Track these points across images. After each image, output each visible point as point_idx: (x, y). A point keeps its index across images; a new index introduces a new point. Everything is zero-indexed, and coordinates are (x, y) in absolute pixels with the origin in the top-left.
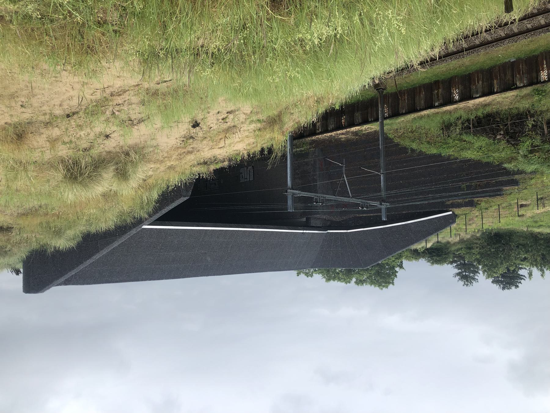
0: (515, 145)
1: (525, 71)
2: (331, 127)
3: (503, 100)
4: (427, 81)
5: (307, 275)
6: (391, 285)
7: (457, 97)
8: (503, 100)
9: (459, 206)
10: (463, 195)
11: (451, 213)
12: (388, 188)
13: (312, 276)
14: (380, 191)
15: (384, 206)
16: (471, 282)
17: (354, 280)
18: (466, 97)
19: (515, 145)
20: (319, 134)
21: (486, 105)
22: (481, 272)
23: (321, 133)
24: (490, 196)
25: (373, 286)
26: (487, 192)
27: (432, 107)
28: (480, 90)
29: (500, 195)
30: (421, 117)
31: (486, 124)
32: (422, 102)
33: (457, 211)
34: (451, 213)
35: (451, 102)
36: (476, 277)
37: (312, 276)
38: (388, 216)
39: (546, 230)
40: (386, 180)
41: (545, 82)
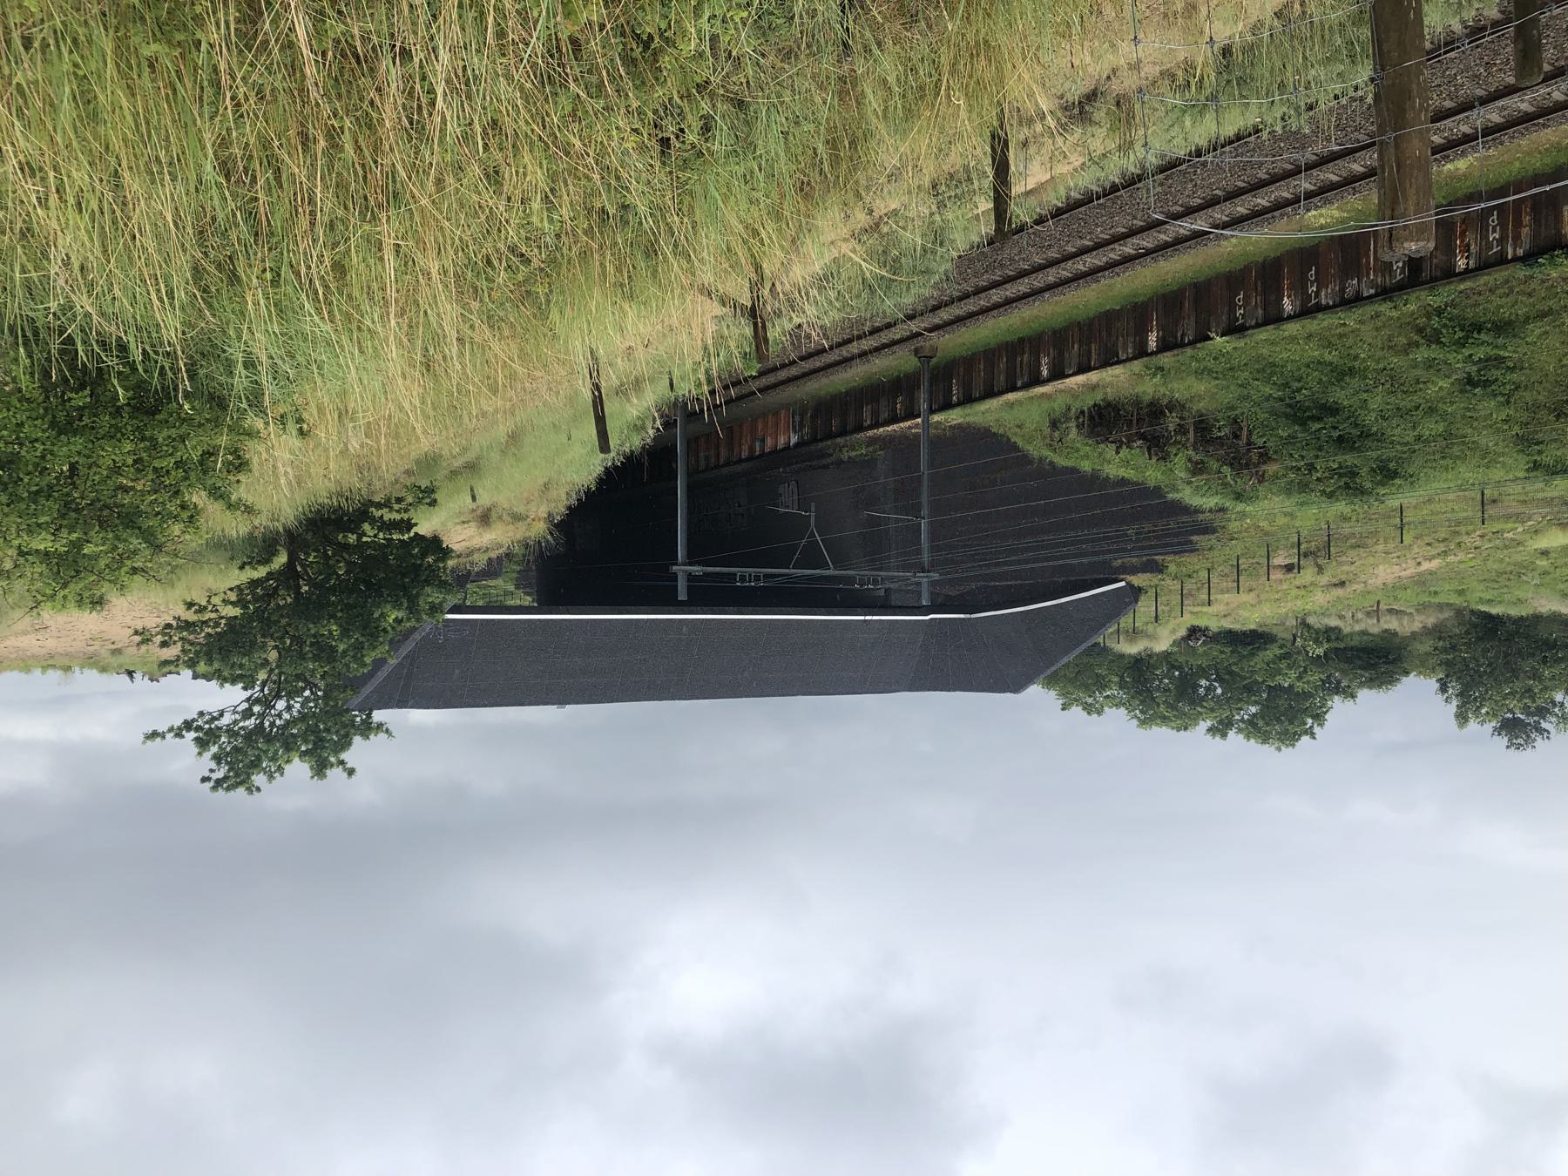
1: (1557, 174)
2: (884, 415)
3: (1116, 380)
5: (1089, 709)
6: (1305, 739)
7: (1045, 373)
8: (1116, 380)
11: (1123, 584)
12: (934, 549)
13: (1100, 712)
14: (919, 552)
15: (924, 579)
18: (1058, 374)
20: (883, 425)
21: (1094, 388)
23: (871, 427)
24: (1175, 553)
27: (1014, 389)
28: (1075, 361)
29: (1192, 551)
30: (1011, 405)
31: (1104, 420)
32: (1002, 378)
33: (1137, 580)
34: (1123, 584)
35: (1037, 381)
36: (1544, 725)
39: (1548, 604)
40: (933, 536)
41: (1153, 353)
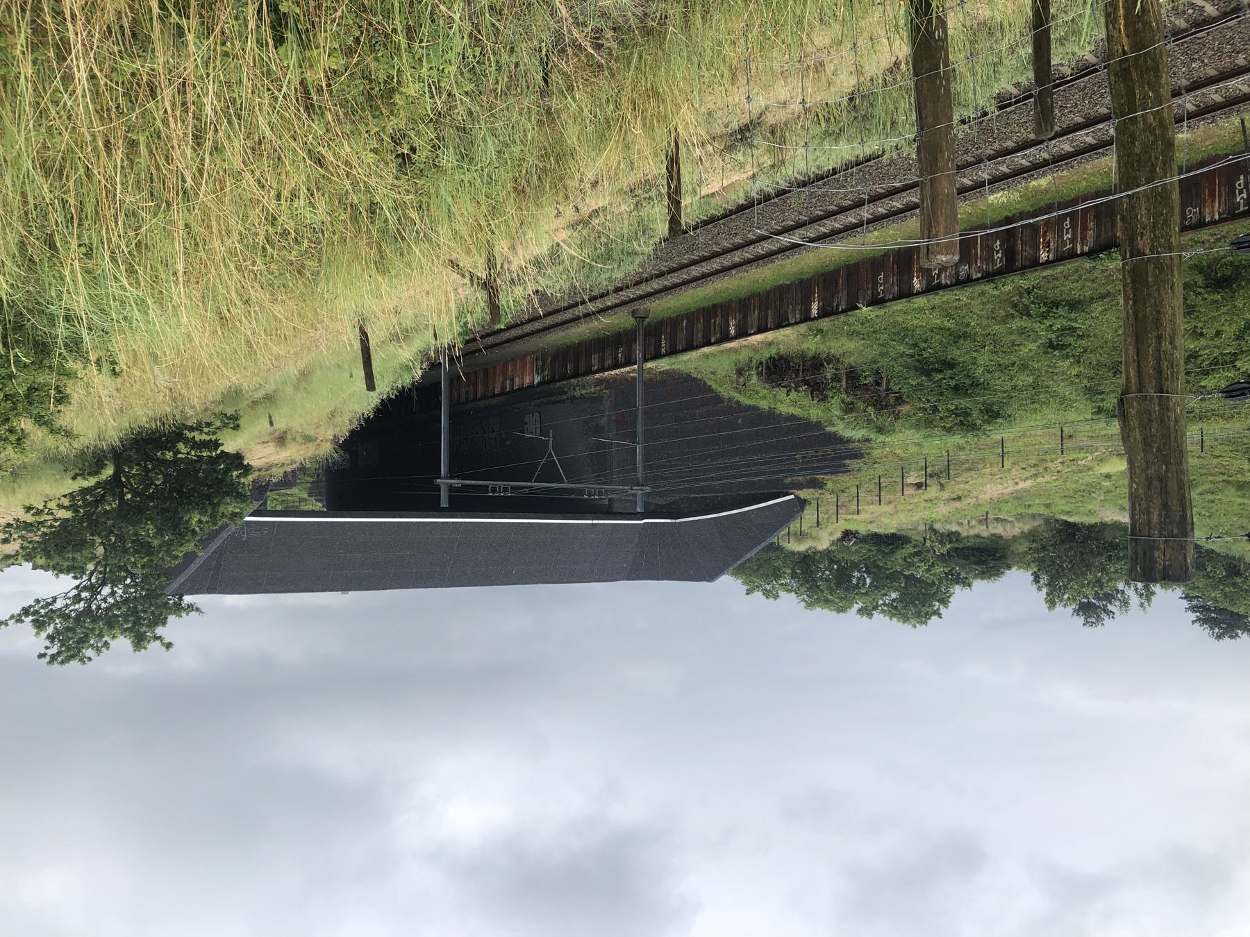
0: (824, 399)
2: (608, 362)
3: (787, 339)
4: (706, 304)
5: (767, 594)
6: (934, 618)
8: (787, 339)
9: (800, 486)
10: (801, 470)
11: (792, 497)
13: (776, 597)
14: (635, 470)
15: (638, 492)
16: (1099, 619)
17: (856, 607)
19: (824, 399)
22: (78, 582)
23: (598, 371)
25: (895, 620)
26: (826, 467)
28: (756, 323)
30: (707, 356)
31: (778, 369)
32: (700, 335)
33: (804, 494)
34: (792, 497)
35: (726, 338)
37: (776, 597)
38: (646, 504)
40: (646, 456)
